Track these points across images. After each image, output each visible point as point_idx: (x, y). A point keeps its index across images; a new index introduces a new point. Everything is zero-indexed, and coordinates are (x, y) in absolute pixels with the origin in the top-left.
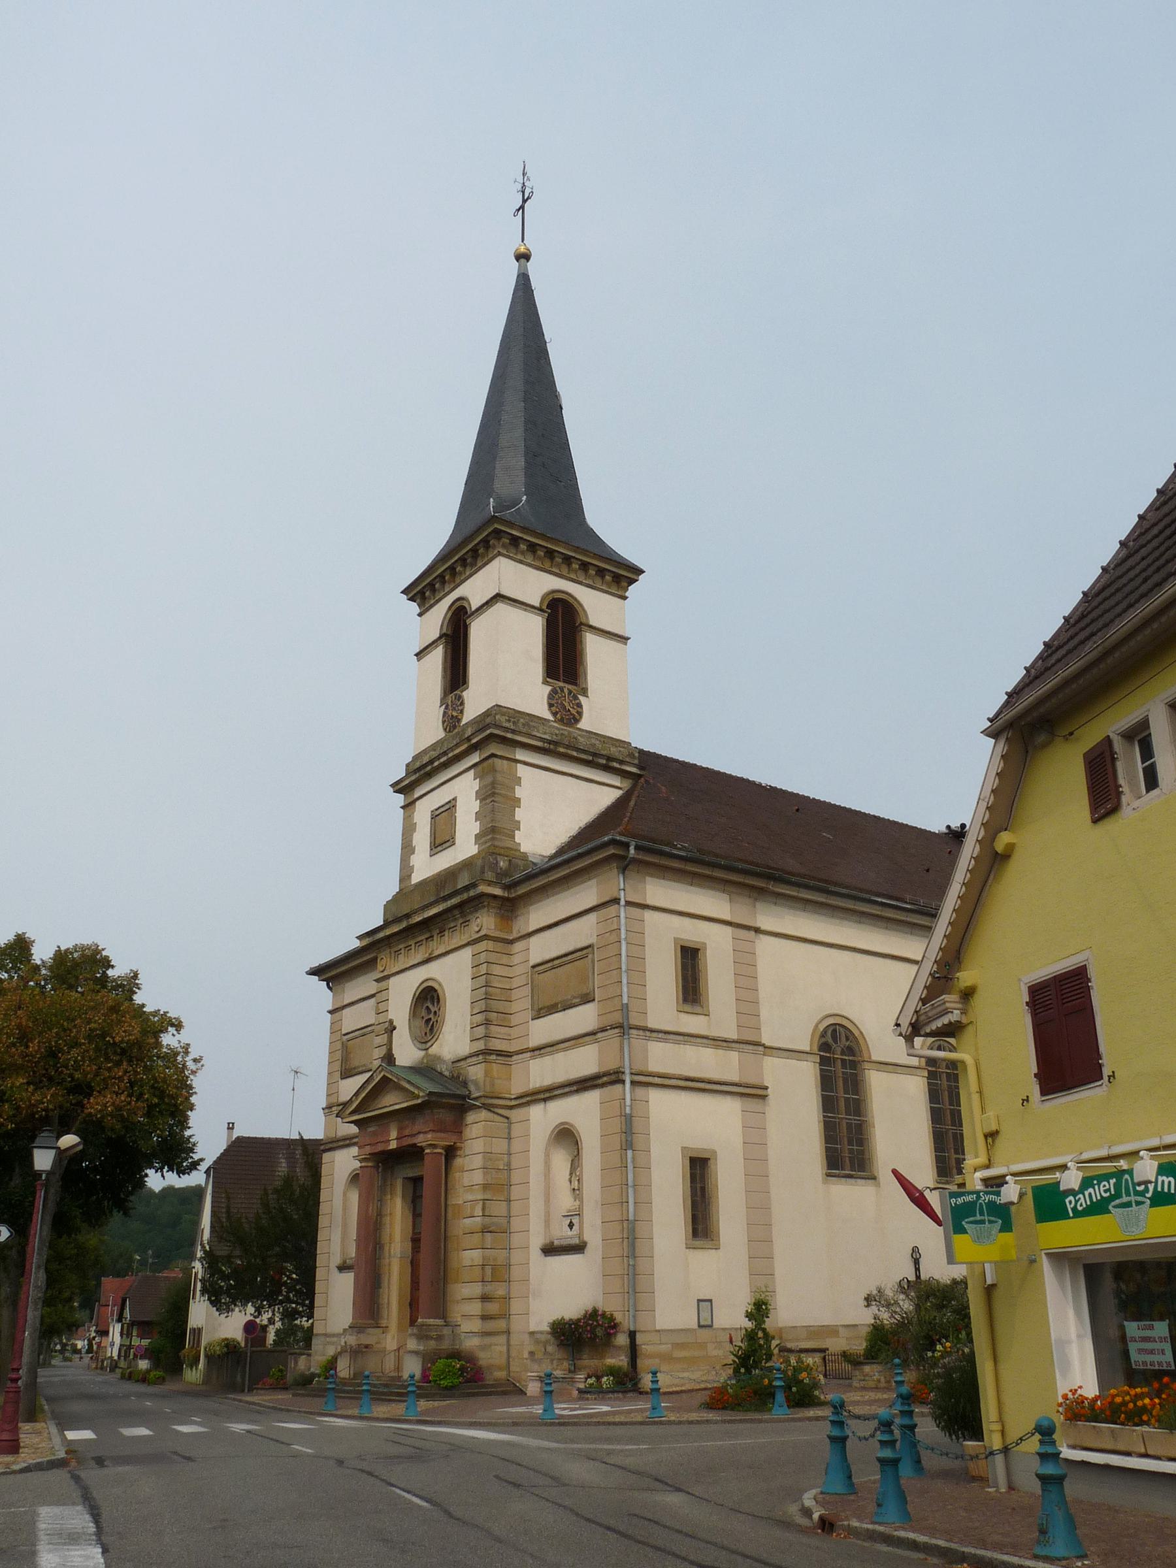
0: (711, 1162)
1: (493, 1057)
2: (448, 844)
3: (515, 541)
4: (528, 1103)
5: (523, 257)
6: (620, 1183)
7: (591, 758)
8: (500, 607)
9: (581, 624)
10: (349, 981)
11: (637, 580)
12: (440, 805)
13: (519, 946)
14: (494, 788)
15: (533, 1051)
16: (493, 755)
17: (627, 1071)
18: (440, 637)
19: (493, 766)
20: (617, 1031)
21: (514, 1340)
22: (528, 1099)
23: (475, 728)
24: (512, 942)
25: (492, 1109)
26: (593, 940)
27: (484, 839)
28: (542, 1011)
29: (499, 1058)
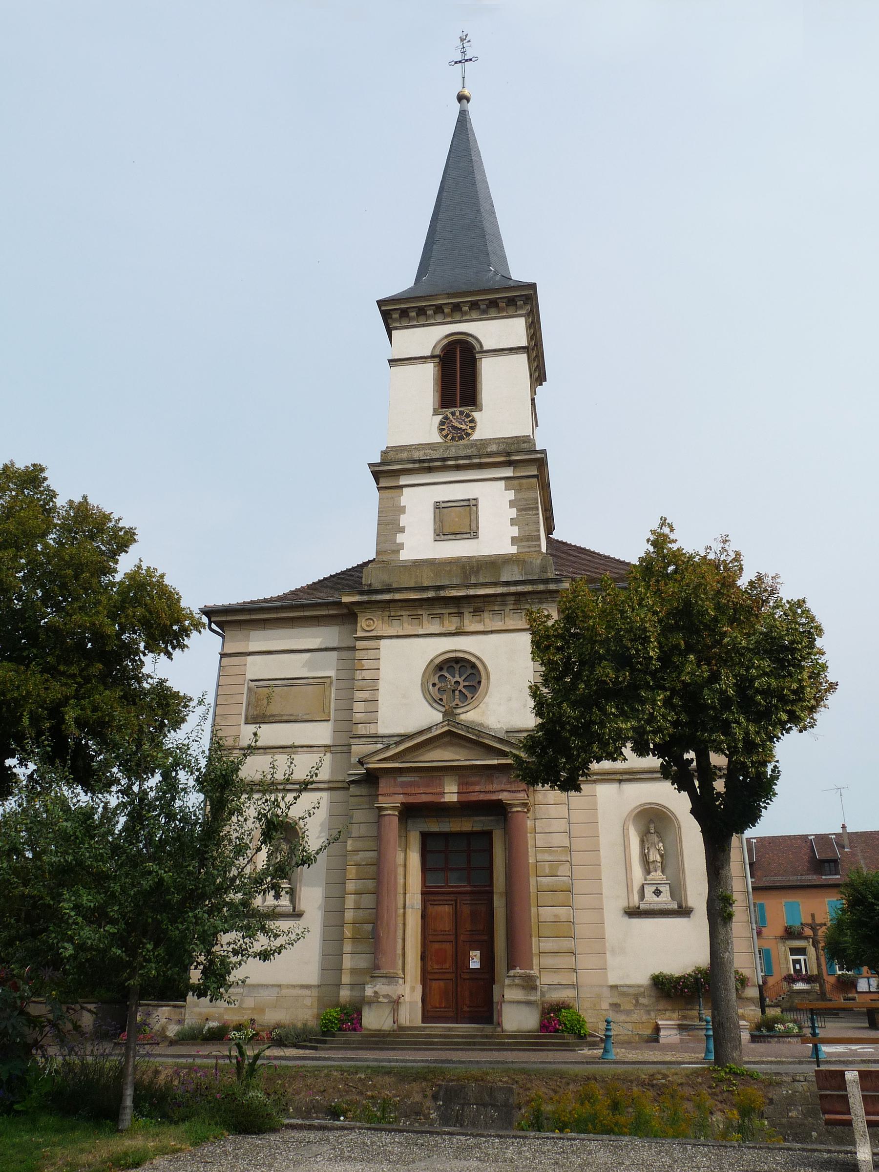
2: (468, 536)
5: (461, 98)
10: (255, 630)
18: (432, 357)
23: (502, 447)
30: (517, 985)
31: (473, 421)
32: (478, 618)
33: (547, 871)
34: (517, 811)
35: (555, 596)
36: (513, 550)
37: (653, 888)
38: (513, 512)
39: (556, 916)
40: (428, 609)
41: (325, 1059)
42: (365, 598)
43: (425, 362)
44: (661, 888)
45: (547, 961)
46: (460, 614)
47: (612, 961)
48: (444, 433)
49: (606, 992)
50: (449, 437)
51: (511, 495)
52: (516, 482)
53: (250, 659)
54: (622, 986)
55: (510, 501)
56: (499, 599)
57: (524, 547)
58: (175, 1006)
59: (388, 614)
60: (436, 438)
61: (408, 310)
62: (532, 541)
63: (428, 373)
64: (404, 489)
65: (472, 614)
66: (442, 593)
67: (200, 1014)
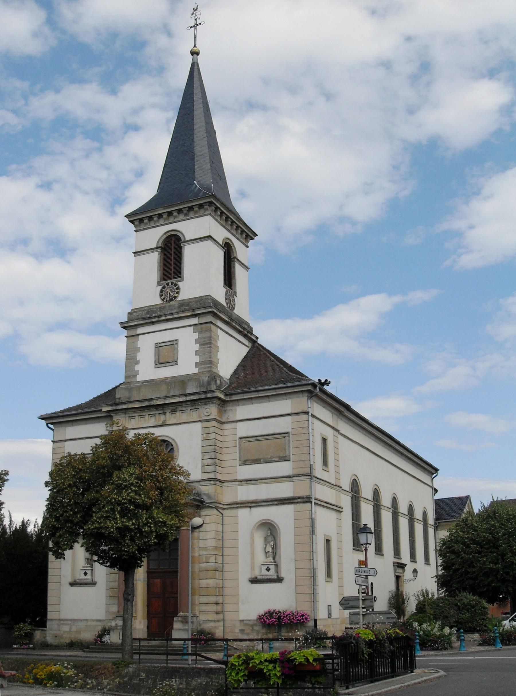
0: (331, 542)
1: (218, 482)
3: (217, 208)
4: (237, 508)
6: (309, 550)
7: (242, 330)
8: (209, 242)
9: (235, 258)
10: (68, 426)
11: (254, 239)
12: (164, 341)
13: (226, 426)
14: (211, 340)
15: (241, 481)
16: (211, 322)
17: (313, 498)
18: (157, 248)
19: (210, 328)
20: (307, 477)
21: (228, 624)
22: (237, 505)
24: (222, 423)
25: (219, 510)
26: (289, 430)
27: (203, 366)
28: (245, 462)
29: (220, 483)
30: (179, 621)
31: (178, 288)
32: (174, 415)
33: (204, 560)
34: (183, 529)
35: (213, 400)
36: (196, 371)
37: (266, 567)
38: (197, 347)
39: (208, 584)
40: (148, 412)
41: (41, 655)
42: (114, 408)
43: (153, 252)
44: (270, 567)
45: (204, 608)
46: (165, 413)
47: (241, 607)
48: (163, 297)
49: (238, 623)
50: (165, 300)
51: (196, 336)
52: (199, 327)
53: (67, 443)
54: (246, 620)
55: (196, 340)
56: (184, 404)
57: (202, 368)
58: (42, 630)
59: (128, 415)
60: (157, 301)
61: (144, 219)
62: (206, 365)
63: (155, 258)
64: (140, 336)
65: (171, 413)
66: (152, 403)
67: (53, 634)
